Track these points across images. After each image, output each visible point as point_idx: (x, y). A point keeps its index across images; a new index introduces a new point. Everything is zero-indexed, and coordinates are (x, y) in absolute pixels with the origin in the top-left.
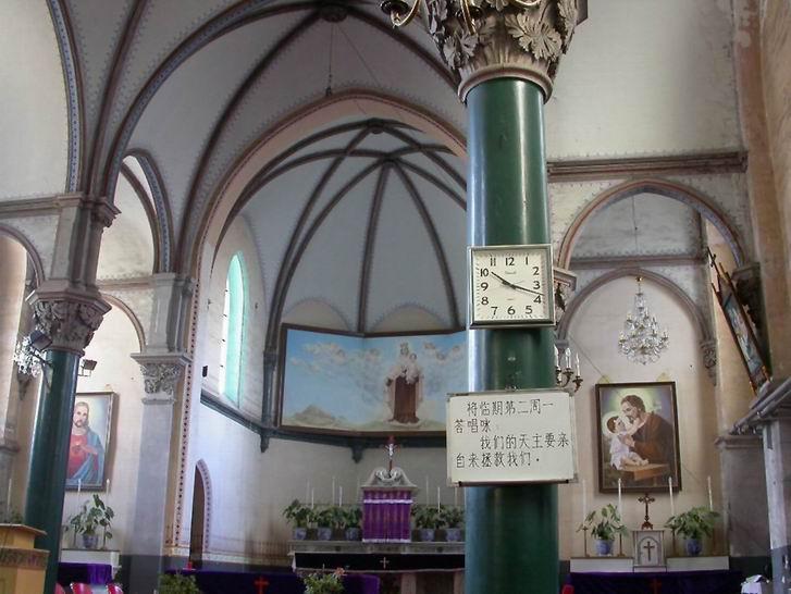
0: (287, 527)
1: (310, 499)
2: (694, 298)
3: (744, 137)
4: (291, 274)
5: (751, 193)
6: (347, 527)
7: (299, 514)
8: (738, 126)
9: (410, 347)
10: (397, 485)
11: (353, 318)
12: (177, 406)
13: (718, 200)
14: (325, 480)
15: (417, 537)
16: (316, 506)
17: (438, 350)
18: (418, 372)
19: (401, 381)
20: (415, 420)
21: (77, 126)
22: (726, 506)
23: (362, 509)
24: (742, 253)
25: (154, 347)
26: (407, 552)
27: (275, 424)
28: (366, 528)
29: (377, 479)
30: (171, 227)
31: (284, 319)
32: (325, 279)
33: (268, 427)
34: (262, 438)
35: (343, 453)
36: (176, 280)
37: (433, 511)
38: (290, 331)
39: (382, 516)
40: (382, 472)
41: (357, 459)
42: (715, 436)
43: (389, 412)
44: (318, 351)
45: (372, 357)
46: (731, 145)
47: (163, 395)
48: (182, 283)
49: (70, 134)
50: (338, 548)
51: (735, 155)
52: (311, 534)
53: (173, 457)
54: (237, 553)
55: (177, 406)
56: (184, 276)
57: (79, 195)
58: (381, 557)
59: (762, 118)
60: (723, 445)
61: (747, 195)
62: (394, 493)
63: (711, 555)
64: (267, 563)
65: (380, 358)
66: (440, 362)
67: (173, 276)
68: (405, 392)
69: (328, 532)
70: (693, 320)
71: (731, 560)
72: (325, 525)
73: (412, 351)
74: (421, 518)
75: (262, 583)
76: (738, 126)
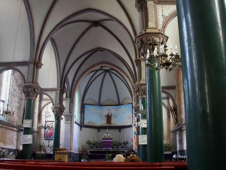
0: (87, 146)
1: (91, 140)
2: (167, 106)
3: (176, 84)
4: (86, 93)
5: (176, 93)
6: (99, 146)
7: (89, 143)
8: (175, 82)
9: (110, 108)
10: (109, 137)
11: (117, 101)
12: (71, 124)
13: (171, 94)
14: (91, 135)
15: (113, 147)
16: (93, 141)
17: (116, 109)
18: (111, 114)
19: (108, 115)
20: (111, 124)
21: (59, 75)
22: (171, 143)
23: (102, 142)
24: (174, 103)
25: (67, 113)
26: (111, 150)
27: (83, 124)
28: (103, 145)
29: (105, 136)
30: (69, 89)
31: (84, 103)
32: (93, 94)
33: (82, 125)
34: (80, 128)
35: (96, 130)
36: (70, 100)
37: (116, 142)
38: (86, 105)
39: (106, 143)
40: (106, 135)
41: (99, 131)
42: (170, 130)
43: (106, 122)
44: (91, 109)
45: (102, 110)
46: (173, 85)
47: (69, 122)
48: (71, 100)
49: (58, 77)
50: (97, 150)
51: (174, 87)
52: (92, 147)
53: (71, 134)
54: (76, 151)
55: (71, 124)
56: (72, 99)
57: (60, 88)
58: (106, 152)
59: (179, 81)
60: (171, 132)
61: (175, 93)
62: (108, 139)
63: (168, 151)
64: (82, 153)
65: (104, 110)
66: (116, 112)
67: (70, 99)
68: (109, 118)
69: (95, 147)
70: (166, 109)
71: (172, 152)
72: (95, 145)
73: (110, 109)
74: (114, 144)
75: (119, 158)
76: (175, 82)
